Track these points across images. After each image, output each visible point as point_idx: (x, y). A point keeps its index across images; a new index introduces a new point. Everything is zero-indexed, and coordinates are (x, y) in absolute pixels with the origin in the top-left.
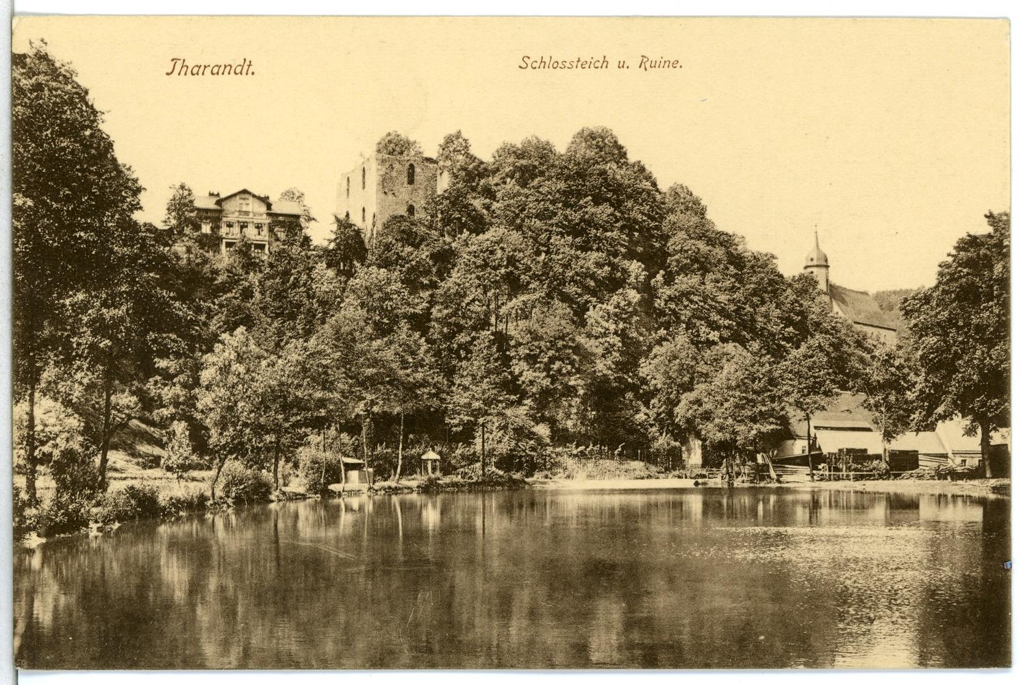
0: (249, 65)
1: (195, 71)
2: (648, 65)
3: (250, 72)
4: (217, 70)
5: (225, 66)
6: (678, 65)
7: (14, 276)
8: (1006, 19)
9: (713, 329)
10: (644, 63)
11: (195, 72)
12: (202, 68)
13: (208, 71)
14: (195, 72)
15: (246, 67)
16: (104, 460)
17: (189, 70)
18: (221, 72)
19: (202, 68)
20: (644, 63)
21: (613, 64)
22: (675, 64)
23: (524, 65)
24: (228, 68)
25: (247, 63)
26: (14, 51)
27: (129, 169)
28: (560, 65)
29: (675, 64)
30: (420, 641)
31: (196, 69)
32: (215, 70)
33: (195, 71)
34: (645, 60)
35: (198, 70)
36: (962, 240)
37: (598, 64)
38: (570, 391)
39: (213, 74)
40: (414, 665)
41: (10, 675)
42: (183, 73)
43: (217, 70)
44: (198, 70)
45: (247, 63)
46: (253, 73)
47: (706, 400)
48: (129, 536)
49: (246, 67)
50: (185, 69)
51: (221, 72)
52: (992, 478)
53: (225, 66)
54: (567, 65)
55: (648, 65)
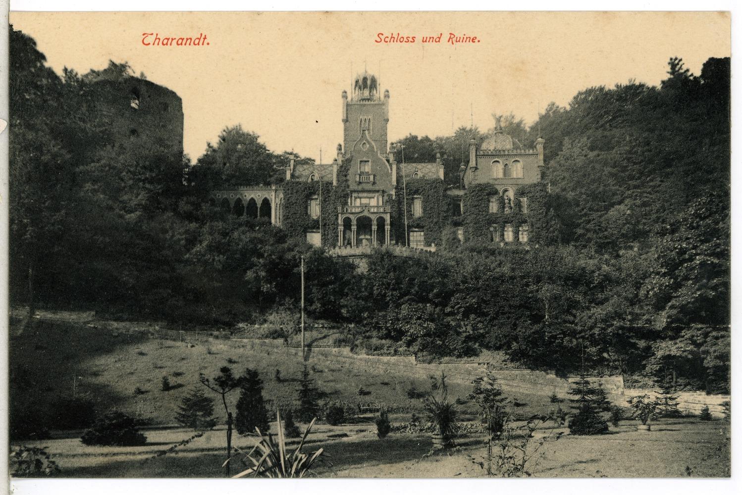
0: (205, 38)
2: (454, 39)
4: (181, 42)
5: (187, 39)
6: (476, 41)
8: (722, 13)
9: (30, 129)
10: (452, 38)
12: (170, 40)
13: (175, 42)
15: (202, 40)
17: (192, 43)
19: (170, 40)
20: (452, 38)
21: (419, 39)
23: (379, 40)
24: (189, 41)
28: (405, 39)
32: (180, 42)
33: (165, 42)
34: (452, 36)
36: (72, 71)
38: (347, 412)
39: (178, 44)
43: (181, 42)
45: (203, 36)
46: (208, 44)
47: (484, 416)
49: (202, 40)
50: (157, 40)
51: (184, 43)
53: (187, 39)
54: (410, 39)
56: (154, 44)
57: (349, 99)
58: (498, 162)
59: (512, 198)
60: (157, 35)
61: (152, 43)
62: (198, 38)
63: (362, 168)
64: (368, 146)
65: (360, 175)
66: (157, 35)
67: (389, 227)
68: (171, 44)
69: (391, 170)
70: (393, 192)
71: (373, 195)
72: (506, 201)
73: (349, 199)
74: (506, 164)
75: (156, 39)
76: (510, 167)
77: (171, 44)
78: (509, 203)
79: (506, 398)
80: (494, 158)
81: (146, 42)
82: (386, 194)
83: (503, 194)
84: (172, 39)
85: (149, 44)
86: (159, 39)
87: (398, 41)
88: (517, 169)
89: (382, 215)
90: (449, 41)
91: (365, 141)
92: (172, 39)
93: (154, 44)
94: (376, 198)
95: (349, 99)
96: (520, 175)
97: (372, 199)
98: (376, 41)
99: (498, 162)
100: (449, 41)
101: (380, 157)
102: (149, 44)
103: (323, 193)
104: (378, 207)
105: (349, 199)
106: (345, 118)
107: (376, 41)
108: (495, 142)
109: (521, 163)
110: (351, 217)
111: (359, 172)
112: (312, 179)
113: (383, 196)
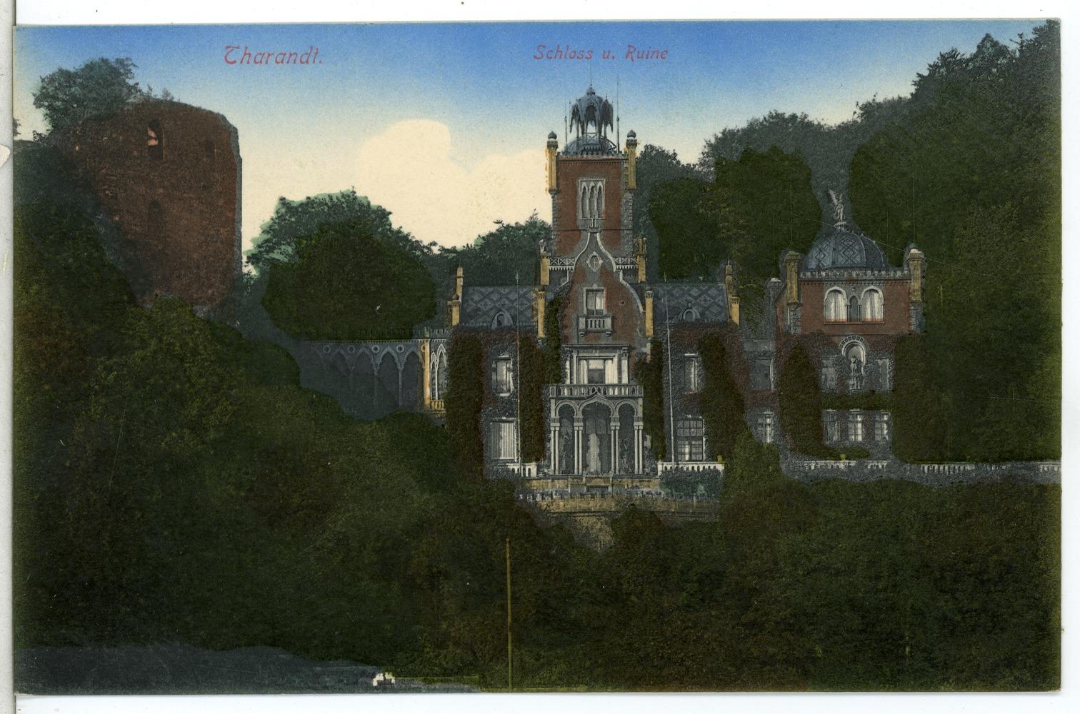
3: (317, 60)
7: (14, 373)
11: (304, 60)
13: (272, 59)
14: (304, 60)
16: (613, 386)
17: (298, 60)
18: (264, 60)
23: (538, 55)
24: (293, 57)
25: (314, 51)
26: (21, 21)
28: (577, 55)
30: (62, 334)
31: (281, 56)
33: (259, 58)
34: (632, 50)
41: (9, 700)
42: (292, 61)
45: (314, 51)
50: (247, 57)
53: (291, 55)
56: (241, 62)
57: (561, 148)
58: (840, 292)
59: (863, 359)
60: (246, 48)
61: (239, 61)
62: (307, 54)
63: (590, 304)
64: (601, 262)
65: (587, 318)
66: (246, 48)
67: (641, 423)
68: (267, 63)
69: (644, 309)
70: (647, 349)
71: (613, 354)
72: (852, 365)
73: (568, 363)
74: (854, 297)
75: (245, 54)
76: (860, 302)
77: (267, 63)
78: (858, 370)
79: (571, 131)
80: (831, 286)
81: (230, 58)
82: (634, 353)
83: (847, 353)
84: (269, 55)
85: (235, 62)
86: (250, 54)
87: (568, 56)
88: (872, 303)
89: (630, 402)
90: (627, 57)
91: (595, 253)
92: (269, 55)
93: (241, 62)
94: (616, 360)
95: (561, 148)
96: (879, 316)
97: (610, 362)
98: (535, 57)
99: (840, 292)
100: (627, 57)
101: (624, 283)
102: (235, 62)
103: (522, 411)
104: (620, 385)
105: (568, 363)
106: (555, 187)
107: (535, 57)
108: (834, 249)
109: (881, 293)
110: (573, 404)
111: (585, 312)
112: (499, 323)
113: (629, 357)
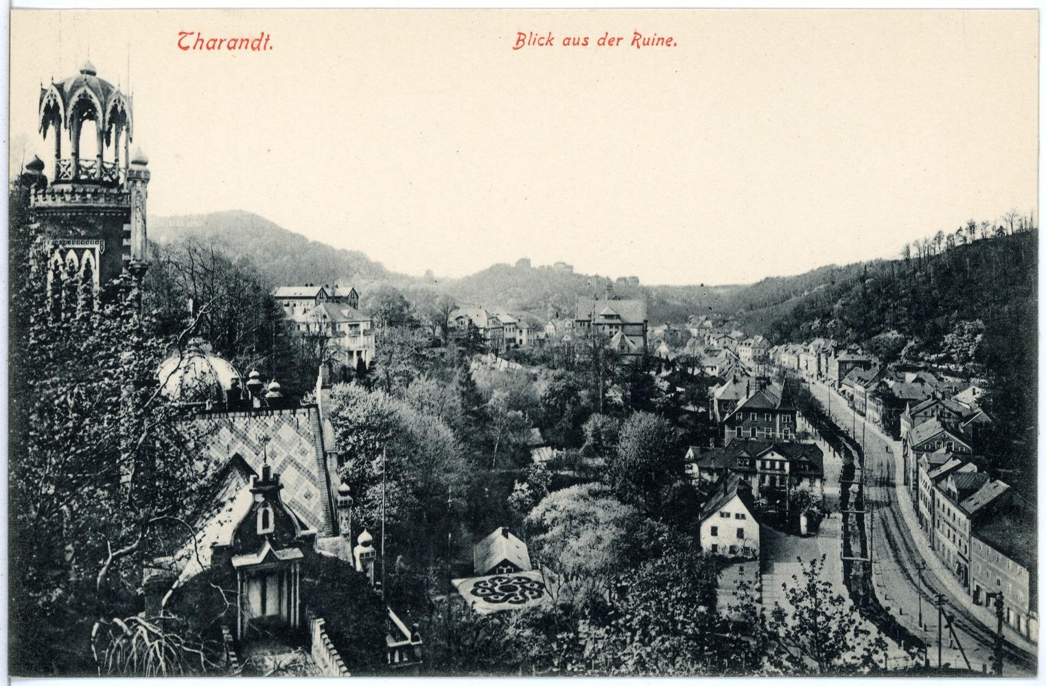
1: (211, 45)
2: (640, 42)
3: (268, 47)
5: (242, 41)
13: (224, 44)
17: (250, 45)
19: (218, 43)
22: (669, 42)
24: (245, 43)
25: (265, 37)
27: (972, 227)
29: (669, 42)
33: (211, 45)
34: (638, 37)
35: (214, 44)
37: (544, 41)
40: (171, 673)
44: (214, 44)
45: (265, 37)
48: (348, 674)
50: (200, 42)
52: (969, 516)
53: (221, 41)
55: (640, 42)
